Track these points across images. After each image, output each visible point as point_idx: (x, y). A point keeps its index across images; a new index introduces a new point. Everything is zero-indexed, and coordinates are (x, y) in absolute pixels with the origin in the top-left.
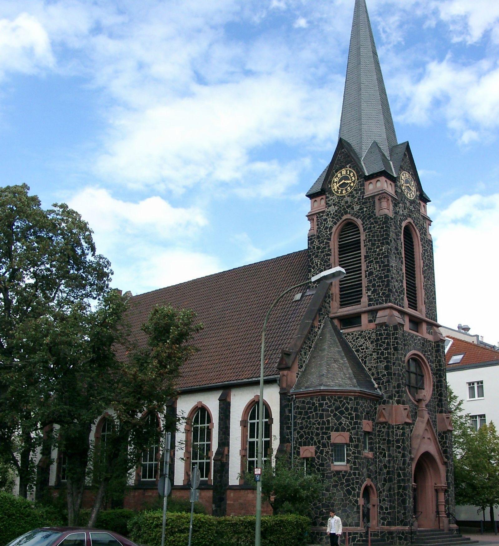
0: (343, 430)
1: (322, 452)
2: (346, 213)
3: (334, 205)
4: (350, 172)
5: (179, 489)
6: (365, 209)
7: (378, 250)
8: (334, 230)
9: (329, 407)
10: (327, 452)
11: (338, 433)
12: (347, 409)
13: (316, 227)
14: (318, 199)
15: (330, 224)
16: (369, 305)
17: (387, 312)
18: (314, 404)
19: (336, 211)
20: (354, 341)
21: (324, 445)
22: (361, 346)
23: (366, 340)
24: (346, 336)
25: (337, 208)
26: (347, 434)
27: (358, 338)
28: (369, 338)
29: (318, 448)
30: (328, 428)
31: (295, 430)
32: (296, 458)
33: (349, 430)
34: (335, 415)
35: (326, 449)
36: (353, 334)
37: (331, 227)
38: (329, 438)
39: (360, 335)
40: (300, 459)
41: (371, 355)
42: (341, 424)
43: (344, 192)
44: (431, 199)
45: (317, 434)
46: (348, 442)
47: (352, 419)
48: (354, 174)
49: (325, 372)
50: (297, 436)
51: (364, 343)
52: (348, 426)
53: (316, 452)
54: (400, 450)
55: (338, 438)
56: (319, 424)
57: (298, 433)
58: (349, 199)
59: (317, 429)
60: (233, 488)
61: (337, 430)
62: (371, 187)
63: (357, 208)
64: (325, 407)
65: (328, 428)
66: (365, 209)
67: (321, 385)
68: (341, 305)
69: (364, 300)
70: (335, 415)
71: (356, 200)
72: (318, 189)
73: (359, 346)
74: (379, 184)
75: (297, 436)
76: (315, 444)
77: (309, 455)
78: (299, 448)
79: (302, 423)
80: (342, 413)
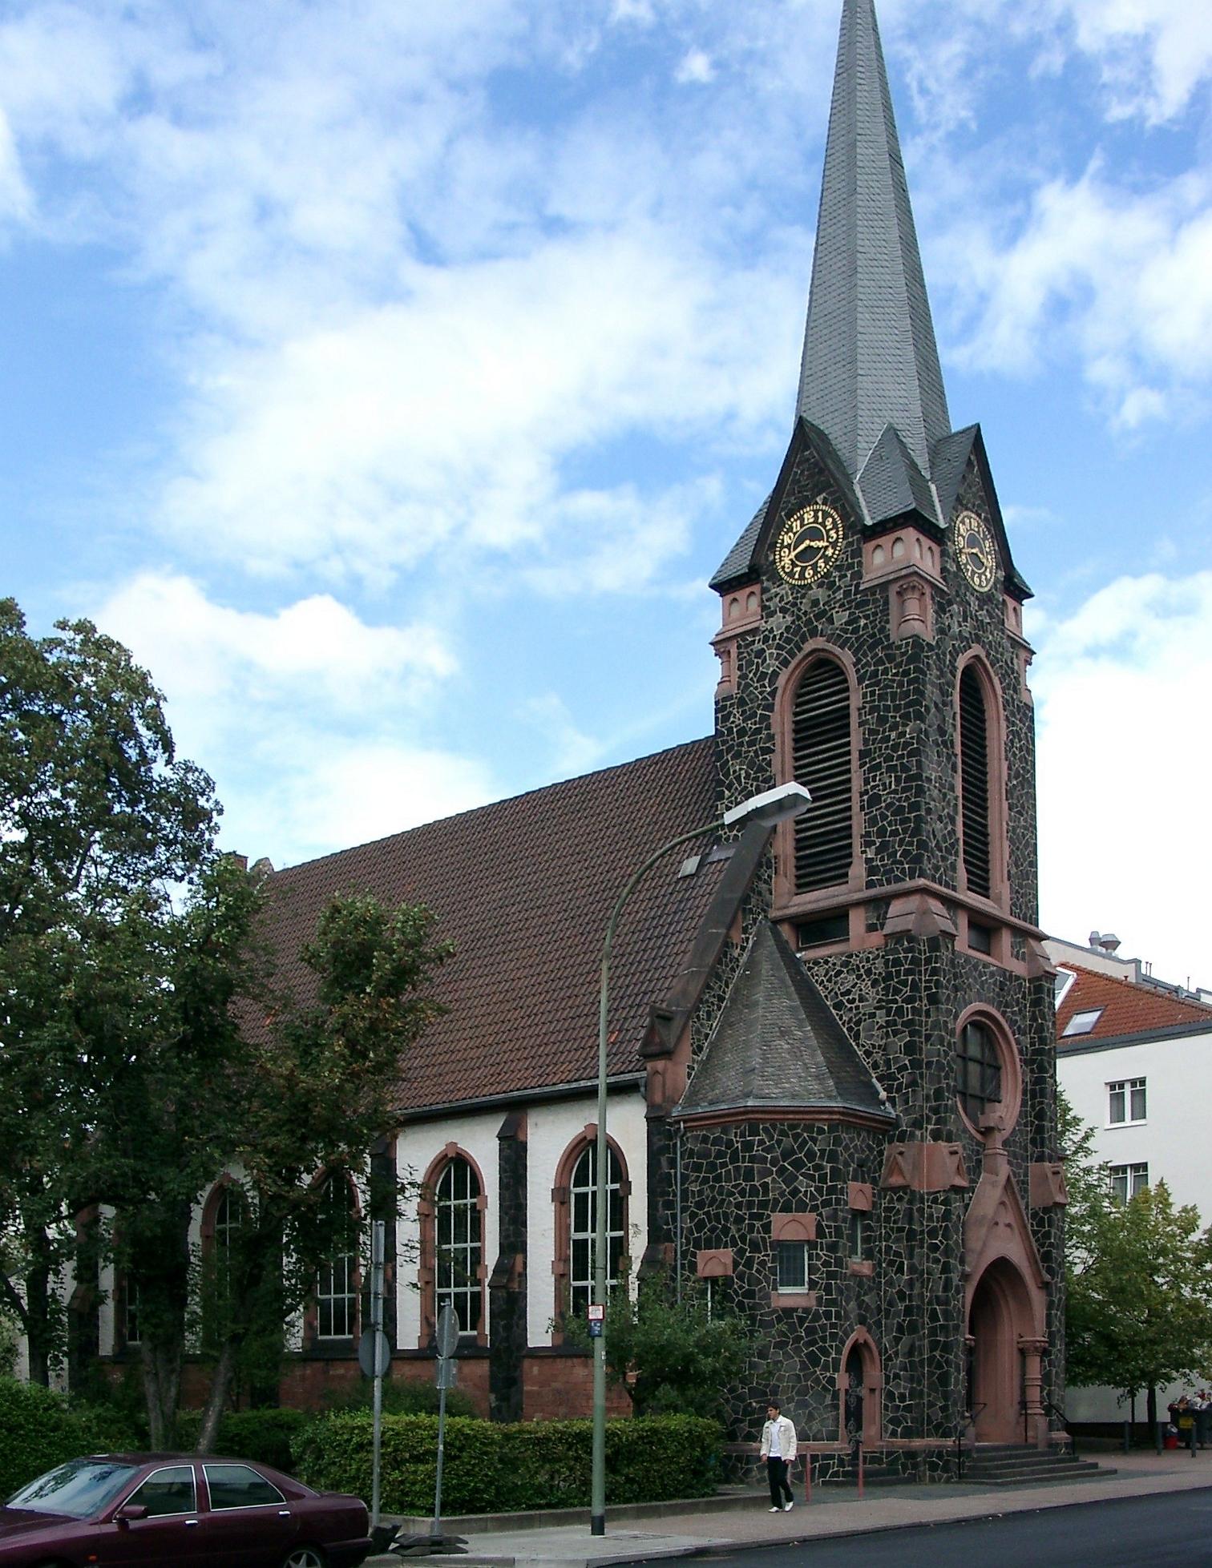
0: (802, 1207)
1: (749, 1263)
2: (814, 633)
6: (862, 622)
7: (893, 735)
8: (781, 681)
9: (768, 1150)
12: (811, 1155)
14: (741, 595)
15: (772, 664)
16: (870, 885)
17: (914, 902)
20: (829, 981)
21: (755, 1247)
22: (848, 992)
23: (859, 977)
24: (810, 969)
28: (869, 972)
30: (763, 1205)
31: (684, 1210)
32: (688, 1279)
33: (814, 1208)
34: (782, 1171)
35: (759, 1256)
36: (826, 962)
38: (767, 1228)
39: (845, 964)
46: (813, 1237)
48: (834, 522)
49: (756, 1062)
50: (688, 1224)
53: (736, 1264)
55: (788, 1227)
56: (742, 1193)
57: (693, 1216)
58: (820, 594)
59: (739, 1206)
60: (538, 1354)
61: (786, 1209)
62: (879, 558)
64: (757, 1150)
65: (763, 1205)
66: (862, 622)
68: (798, 886)
69: (858, 870)
70: (782, 1171)
71: (840, 595)
72: (742, 566)
73: (843, 994)
74: (899, 550)
75: (688, 1224)
77: (718, 1271)
78: (694, 1255)
79: (700, 1192)
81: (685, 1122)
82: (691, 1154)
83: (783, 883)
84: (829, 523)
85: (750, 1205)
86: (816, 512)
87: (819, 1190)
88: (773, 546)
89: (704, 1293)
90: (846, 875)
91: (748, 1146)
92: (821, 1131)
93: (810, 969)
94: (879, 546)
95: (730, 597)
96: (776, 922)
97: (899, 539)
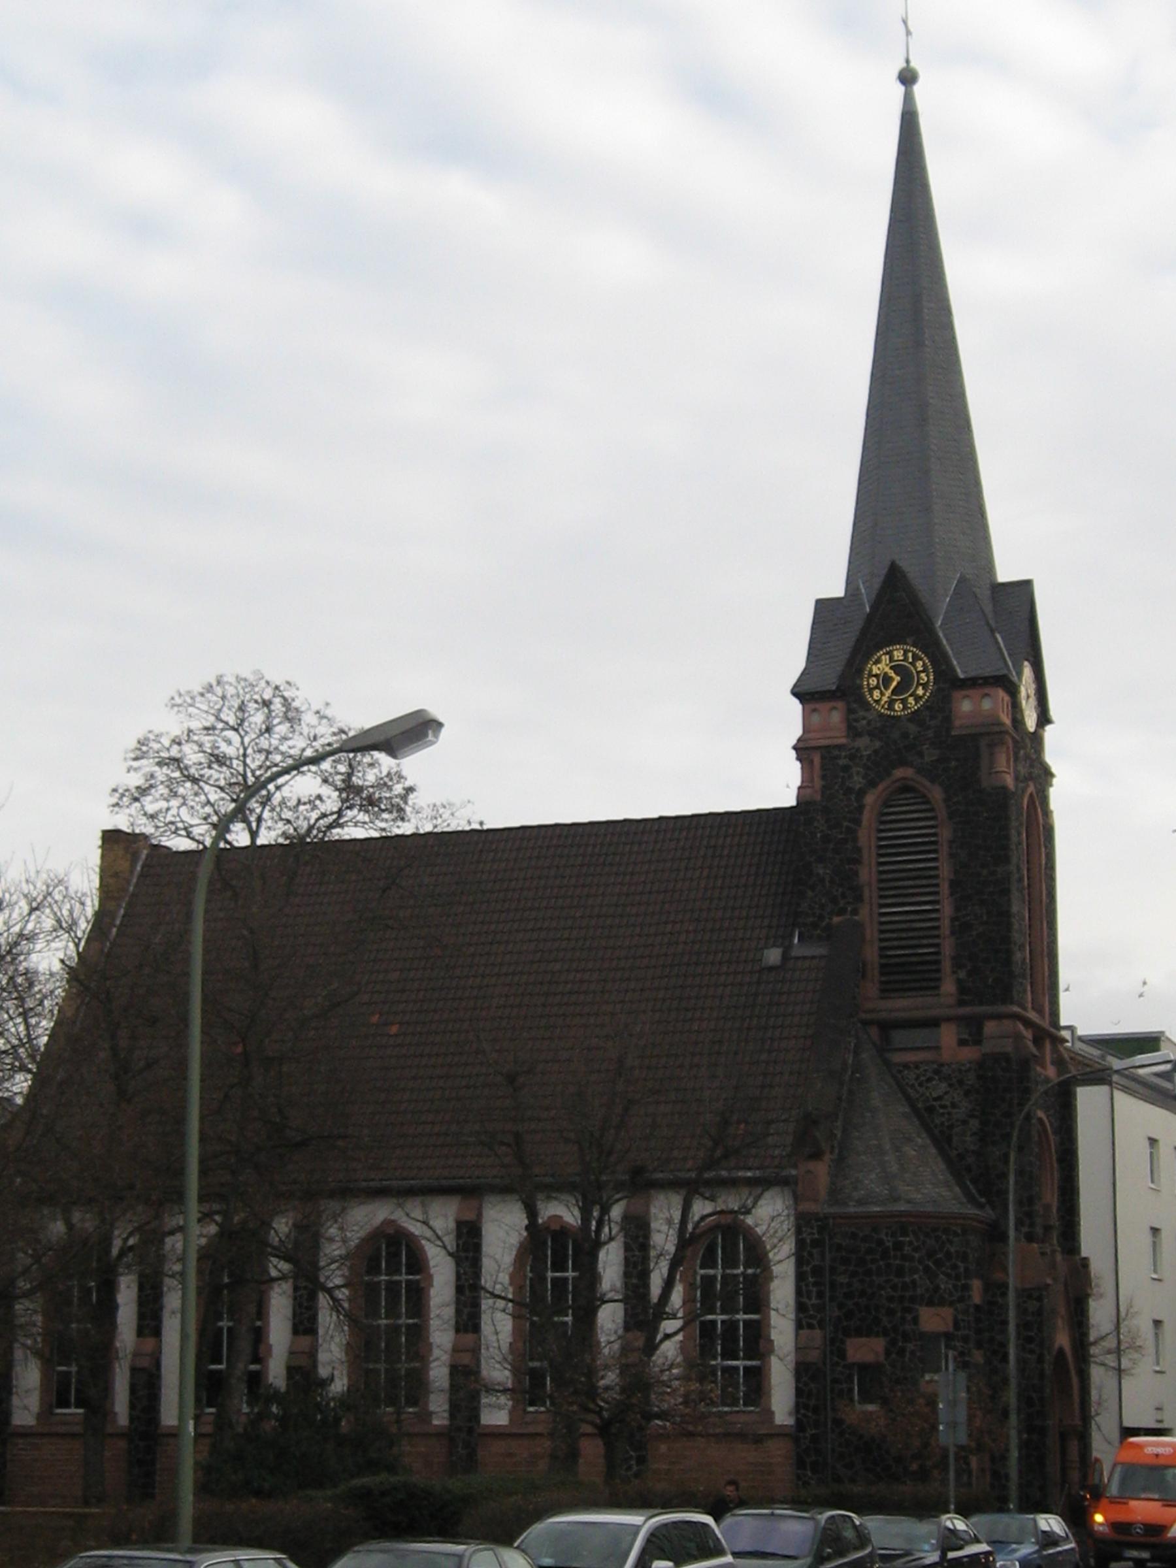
0: (942, 1303)
1: (901, 1352)
2: (903, 763)
3: (871, 734)
4: (916, 658)
5: (501, 1434)
6: (953, 764)
7: (985, 872)
8: (869, 799)
9: (916, 1249)
10: (912, 1353)
11: (932, 1310)
12: (948, 1255)
13: (818, 783)
14: (824, 706)
15: (858, 781)
16: (961, 1003)
17: (1007, 1025)
18: (880, 1242)
19: (876, 752)
20: (921, 1085)
21: (906, 1337)
22: (939, 1098)
23: (950, 1085)
24: (900, 1072)
25: (878, 744)
26: (947, 1312)
27: (929, 1080)
28: (961, 1082)
29: (893, 1343)
30: (913, 1299)
31: (832, 1299)
32: (837, 1364)
33: (951, 1304)
34: (927, 1269)
35: (910, 1346)
36: (917, 1067)
37: (861, 793)
38: (916, 1320)
39: (937, 1072)
40: (845, 1366)
41: (964, 1122)
42: (937, 1288)
43: (898, 706)
44: (887, 564)
45: (891, 1313)
46: (951, 1329)
47: (957, 1278)
48: (924, 665)
49: (894, 1168)
50: (837, 1313)
51: (946, 1093)
52: (951, 1294)
53: (888, 1353)
54: (1032, 1346)
55: (933, 1320)
56: (894, 1288)
57: (841, 1306)
58: (913, 729)
59: (890, 1299)
60: (25, 1433)
61: (930, 1303)
62: (966, 706)
63: (931, 755)
64: (907, 1250)
65: (913, 1299)
66: (953, 764)
67: (896, 1200)
68: (883, 991)
69: (949, 987)
70: (927, 1269)
71: (930, 734)
72: (831, 683)
73: (935, 1099)
74: (987, 705)
75: (837, 1313)
76: (885, 1333)
77: (869, 1358)
78: (843, 1342)
79: (849, 1285)
80: (938, 1263)
81: (834, 1218)
82: (839, 1247)
83: (871, 988)
84: (919, 664)
85: (902, 1298)
86: (906, 652)
87: (955, 1286)
88: (860, 672)
89: (850, 1379)
90: (937, 988)
91: (898, 1246)
92: (956, 1234)
93: (900, 1072)
94: (968, 696)
95: (812, 706)
96: (866, 1023)
97: (987, 695)
